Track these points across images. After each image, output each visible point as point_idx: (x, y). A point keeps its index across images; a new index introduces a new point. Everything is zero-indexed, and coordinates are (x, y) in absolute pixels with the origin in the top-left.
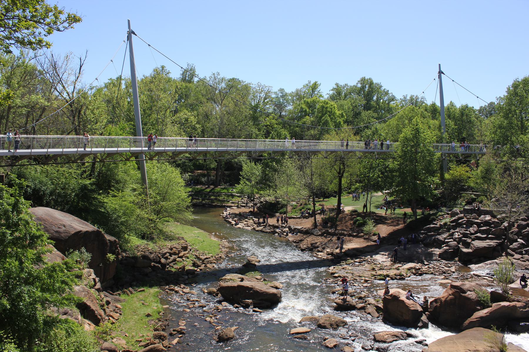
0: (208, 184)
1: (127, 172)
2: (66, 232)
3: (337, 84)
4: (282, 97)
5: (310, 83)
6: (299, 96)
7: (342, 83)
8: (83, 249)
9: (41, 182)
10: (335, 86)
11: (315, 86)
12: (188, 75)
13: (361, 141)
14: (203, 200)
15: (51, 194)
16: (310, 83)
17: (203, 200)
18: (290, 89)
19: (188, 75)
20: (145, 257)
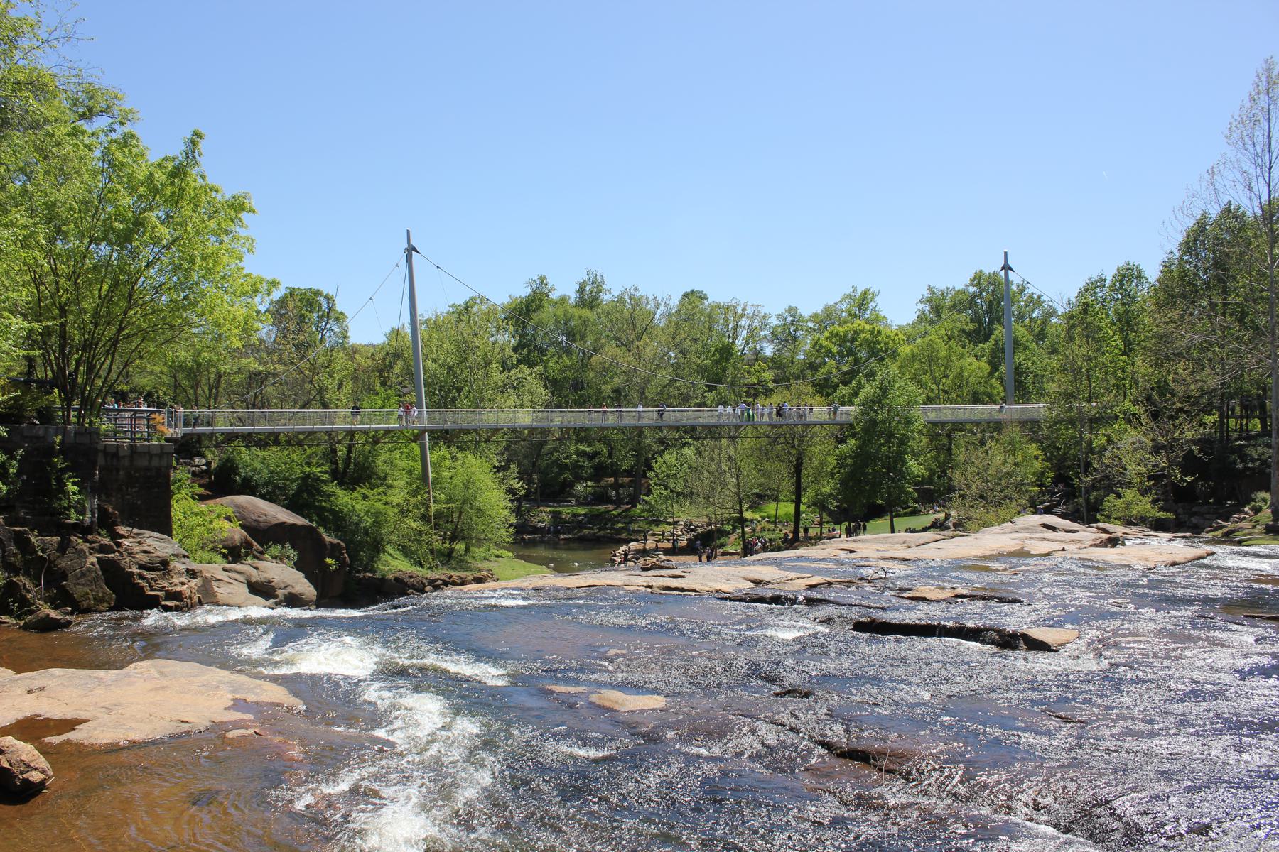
0: (618, 503)
1: (394, 463)
2: (265, 521)
3: (930, 289)
4: (792, 323)
5: (855, 291)
6: (827, 316)
7: (940, 286)
8: (288, 545)
9: (254, 470)
10: (927, 294)
11: (863, 301)
12: (589, 297)
13: (521, 406)
14: (600, 529)
15: (266, 484)
16: (855, 291)
17: (600, 529)
18: (809, 307)
19: (589, 297)
20: (397, 579)
